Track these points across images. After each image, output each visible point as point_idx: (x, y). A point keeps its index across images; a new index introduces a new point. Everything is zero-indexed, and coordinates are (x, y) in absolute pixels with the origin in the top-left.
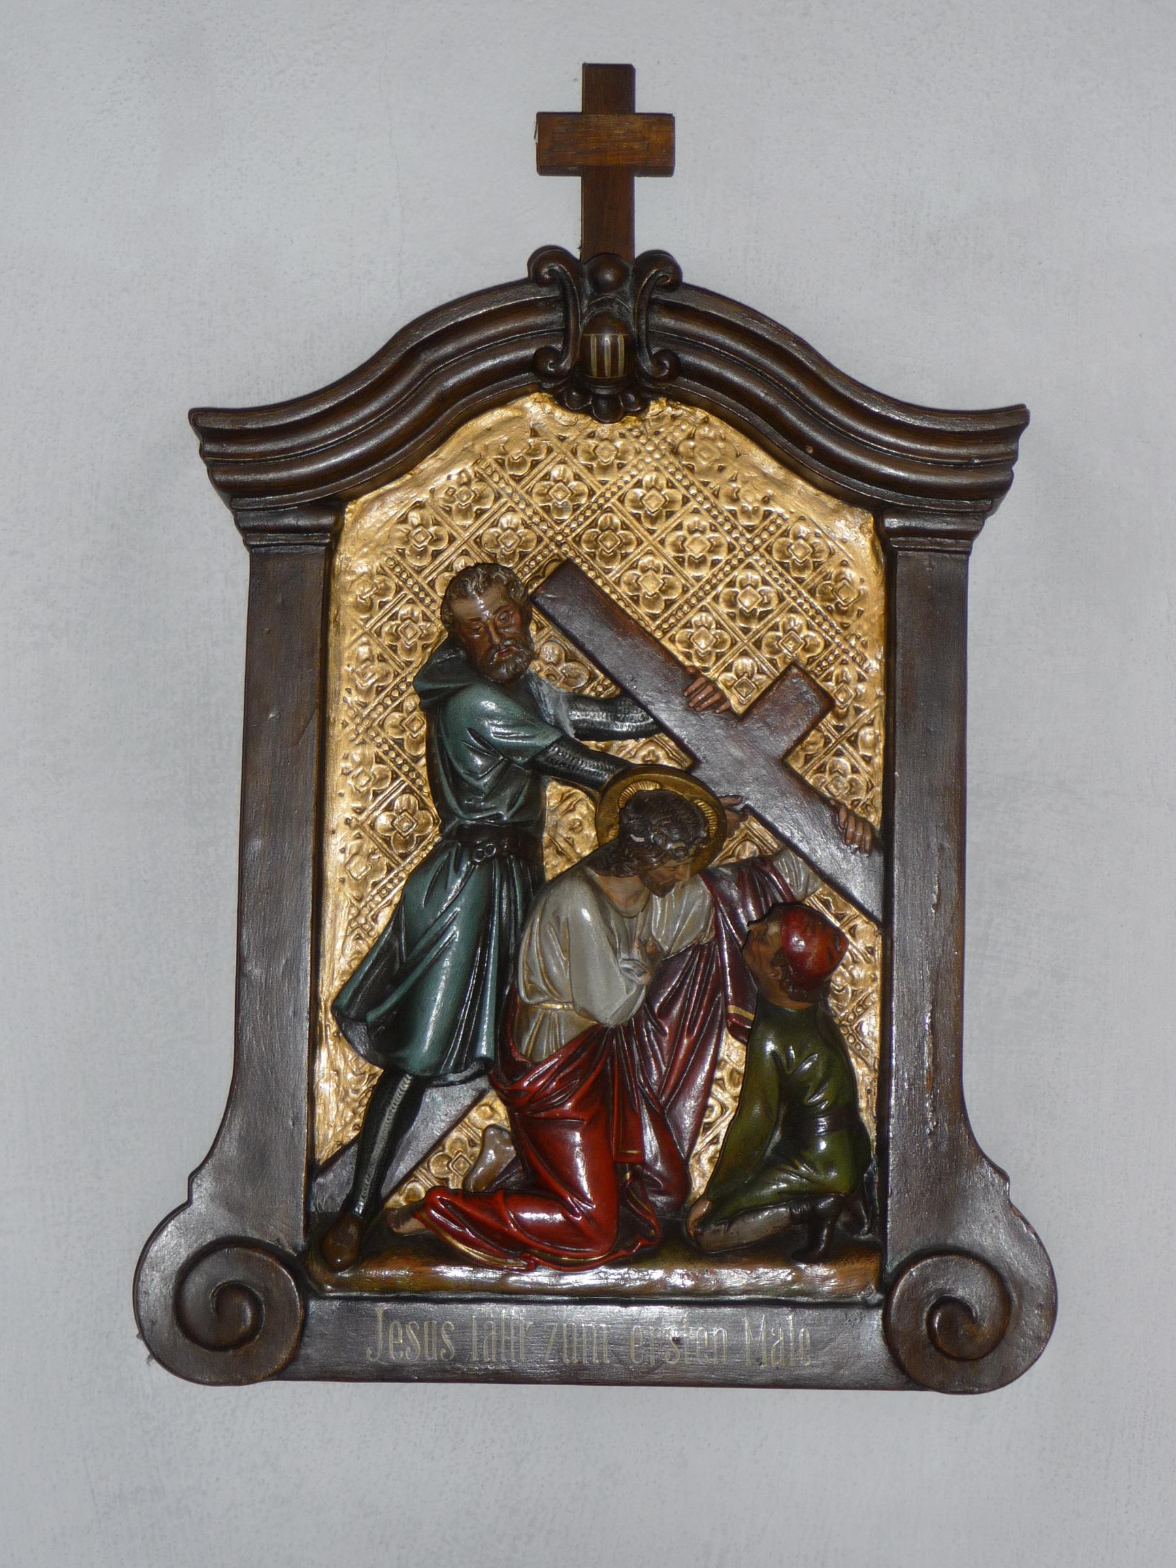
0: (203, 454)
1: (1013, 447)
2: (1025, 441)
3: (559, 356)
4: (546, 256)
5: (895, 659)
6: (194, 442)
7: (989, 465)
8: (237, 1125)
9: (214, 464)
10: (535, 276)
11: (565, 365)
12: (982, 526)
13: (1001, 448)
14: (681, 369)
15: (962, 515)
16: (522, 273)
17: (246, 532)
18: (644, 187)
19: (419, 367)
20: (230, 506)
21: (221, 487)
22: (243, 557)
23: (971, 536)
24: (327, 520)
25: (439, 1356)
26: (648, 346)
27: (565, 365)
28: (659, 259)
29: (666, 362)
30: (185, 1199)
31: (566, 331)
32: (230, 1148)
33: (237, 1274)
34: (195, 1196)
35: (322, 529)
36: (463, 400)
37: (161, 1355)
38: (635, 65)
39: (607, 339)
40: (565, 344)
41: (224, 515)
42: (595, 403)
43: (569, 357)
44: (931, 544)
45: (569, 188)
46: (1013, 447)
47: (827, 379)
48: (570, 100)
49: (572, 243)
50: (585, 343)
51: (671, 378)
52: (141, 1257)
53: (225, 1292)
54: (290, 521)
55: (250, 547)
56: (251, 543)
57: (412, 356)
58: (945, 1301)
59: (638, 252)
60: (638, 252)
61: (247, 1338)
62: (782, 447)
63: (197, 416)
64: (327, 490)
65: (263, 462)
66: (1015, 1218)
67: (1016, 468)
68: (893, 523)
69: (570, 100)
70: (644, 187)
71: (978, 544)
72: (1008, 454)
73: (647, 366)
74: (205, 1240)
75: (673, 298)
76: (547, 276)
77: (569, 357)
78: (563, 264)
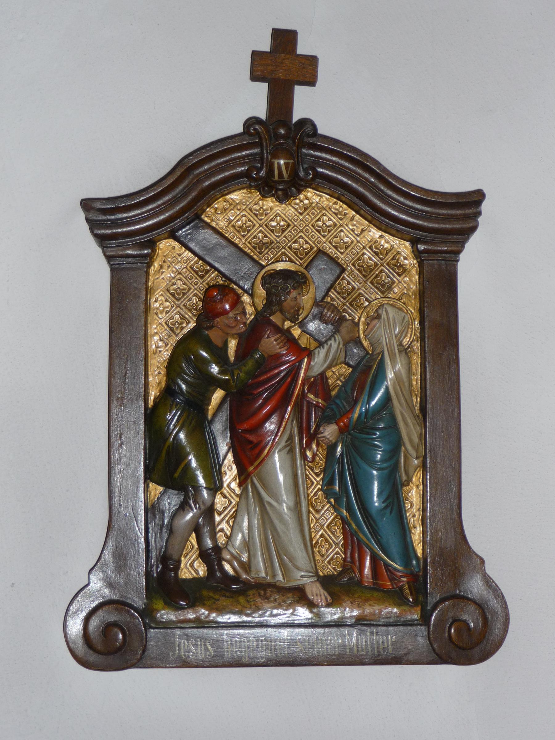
0: (87, 220)
2: (485, 206)
3: (259, 170)
4: (250, 123)
5: (423, 268)
6: (81, 216)
7: (466, 218)
8: (110, 546)
9: (93, 224)
11: (262, 173)
12: (463, 247)
14: (318, 175)
16: (240, 130)
17: (109, 258)
18: (299, 91)
21: (96, 236)
23: (458, 252)
27: (262, 173)
28: (304, 122)
29: (310, 172)
31: (262, 158)
32: (108, 556)
33: (113, 618)
34: (91, 581)
35: (146, 256)
39: (282, 162)
41: (99, 251)
42: (276, 192)
44: (440, 257)
45: (264, 87)
48: (265, 46)
49: (262, 114)
50: (272, 164)
51: (313, 179)
52: (104, 544)
54: (130, 252)
55: (111, 266)
59: (295, 119)
61: (119, 649)
62: (367, 210)
65: (384, 198)
66: (488, 581)
67: (480, 219)
68: (421, 247)
69: (265, 46)
70: (299, 91)
71: (462, 256)
73: (302, 174)
78: (260, 125)
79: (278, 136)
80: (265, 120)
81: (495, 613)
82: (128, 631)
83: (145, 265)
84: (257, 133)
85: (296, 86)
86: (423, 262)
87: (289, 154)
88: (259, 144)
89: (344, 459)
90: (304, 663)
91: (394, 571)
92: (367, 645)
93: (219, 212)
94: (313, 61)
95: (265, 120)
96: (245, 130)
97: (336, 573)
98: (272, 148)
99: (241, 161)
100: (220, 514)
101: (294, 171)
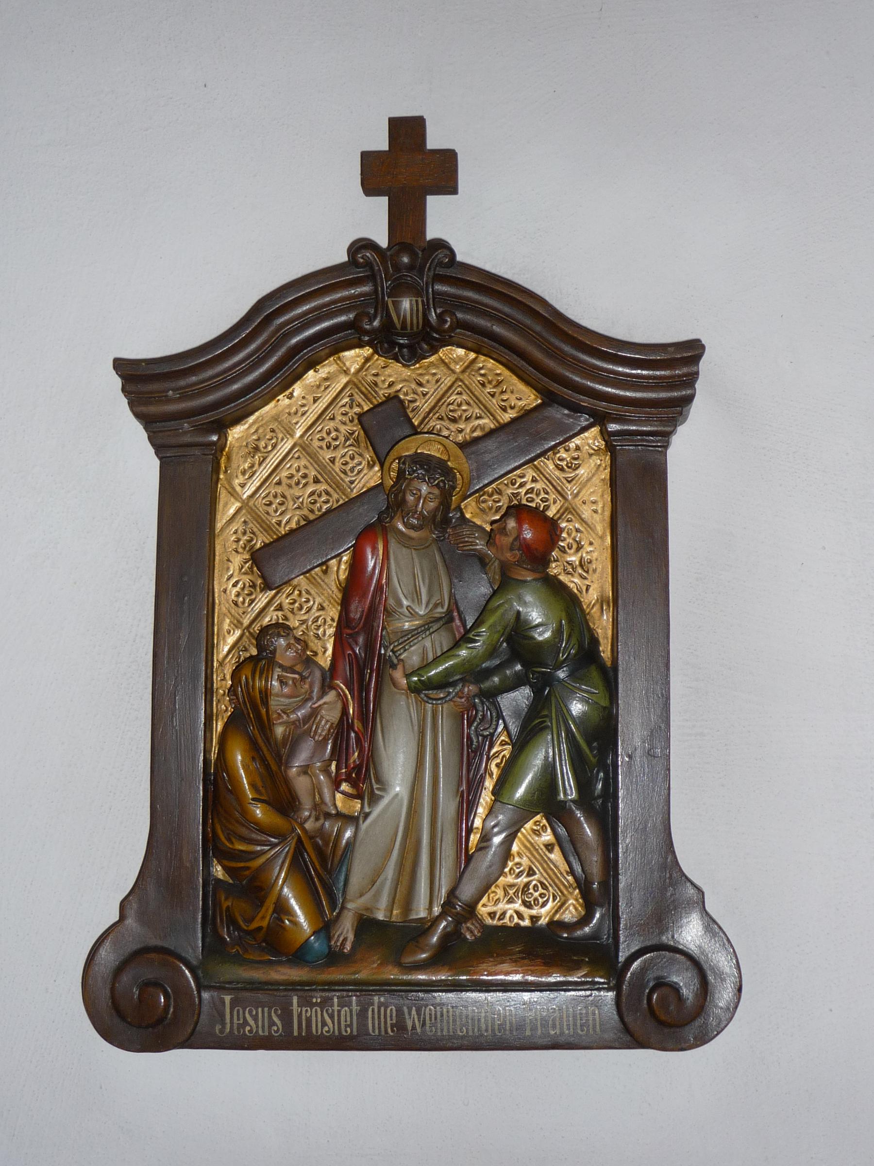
1: (694, 369)
2: (704, 365)
11: (376, 323)
13: (685, 370)
16: (343, 258)
17: (159, 448)
18: (432, 201)
19: (272, 328)
20: (146, 429)
22: (157, 462)
23: (666, 436)
25: (270, 1032)
27: (376, 323)
28: (441, 245)
33: (149, 974)
36: (243, 399)
37: (107, 1034)
43: (378, 319)
46: (694, 369)
47: (560, 325)
48: (381, 142)
51: (452, 328)
53: (147, 985)
57: (269, 319)
58: (661, 984)
63: (120, 365)
64: (212, 416)
66: (711, 925)
67: (697, 386)
68: (613, 427)
69: (381, 142)
70: (432, 201)
75: (450, 272)
76: (361, 260)
77: (378, 319)
79: (397, 267)
81: (721, 976)
84: (368, 264)
85: (428, 197)
87: (416, 291)
88: (372, 278)
89: (483, 764)
90: (360, 1047)
96: (351, 258)
97: (236, 1033)
98: (391, 284)
100: (449, 460)
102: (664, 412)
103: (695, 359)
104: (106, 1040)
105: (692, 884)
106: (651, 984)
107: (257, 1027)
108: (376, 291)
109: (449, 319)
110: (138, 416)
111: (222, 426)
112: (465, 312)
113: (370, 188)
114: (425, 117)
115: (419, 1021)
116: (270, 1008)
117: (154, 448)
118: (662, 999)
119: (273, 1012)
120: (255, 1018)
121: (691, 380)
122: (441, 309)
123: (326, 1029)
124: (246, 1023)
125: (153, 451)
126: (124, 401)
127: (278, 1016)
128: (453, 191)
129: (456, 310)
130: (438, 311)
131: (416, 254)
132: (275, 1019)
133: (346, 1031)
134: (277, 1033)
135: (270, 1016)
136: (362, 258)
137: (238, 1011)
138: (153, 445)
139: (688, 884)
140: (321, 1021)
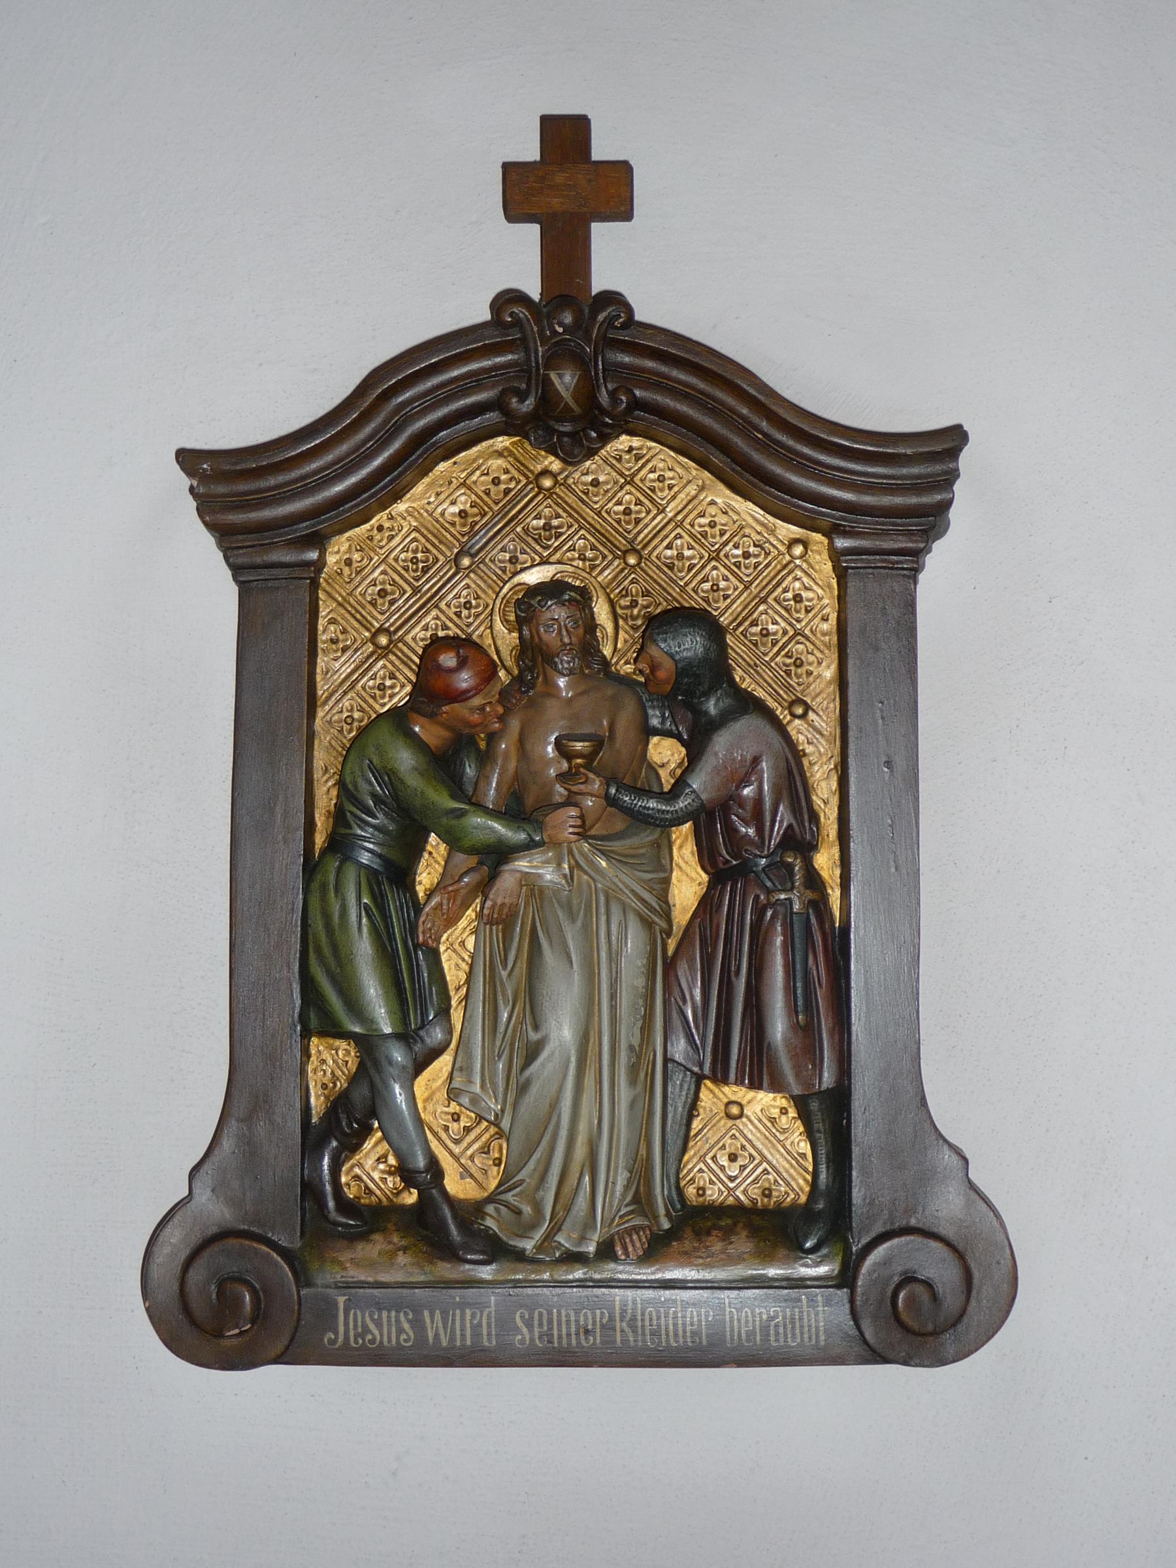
2: (965, 460)
4: (507, 299)
9: (207, 507)
10: (496, 321)
13: (938, 468)
14: (637, 404)
15: (910, 534)
16: (485, 315)
17: (237, 570)
18: (600, 231)
22: (234, 590)
23: (917, 555)
24: (314, 555)
26: (605, 382)
28: (612, 299)
30: (187, 1193)
35: (307, 564)
38: (540, 115)
40: (529, 384)
45: (533, 231)
47: (774, 408)
48: (530, 151)
56: (241, 579)
58: (909, 1279)
60: (595, 290)
63: (187, 459)
64: (304, 528)
65: (769, 446)
68: (841, 543)
69: (530, 151)
70: (600, 231)
72: (946, 473)
73: (604, 398)
74: (774, 1099)
80: (537, 300)
82: (265, 1292)
83: (308, 581)
84: (517, 323)
85: (593, 225)
86: (847, 571)
87: (580, 361)
88: (523, 343)
91: (372, 907)
92: (700, 1321)
93: (753, 874)
94: (622, 171)
95: (537, 300)
99: (475, 381)
101: (587, 391)
102: (914, 524)
103: (953, 453)
104: (177, 1356)
105: (952, 1147)
106: (896, 1279)
107: (381, 1336)
108: (528, 359)
109: (624, 398)
110: (210, 527)
111: (318, 540)
112: (646, 389)
113: (514, 211)
114: (589, 117)
115: (445, 1328)
116: (398, 1312)
117: (231, 570)
118: (910, 1299)
119: (367, 1314)
120: (379, 1325)
121: (948, 479)
122: (615, 385)
123: (403, 1336)
124: (366, 1330)
125: (229, 573)
126: (192, 504)
127: (409, 1321)
128: (627, 215)
129: (634, 387)
130: (610, 386)
131: (581, 311)
132: (406, 1326)
133: (356, 1342)
134: (371, 1344)
135: (398, 1321)
136: (511, 315)
137: (355, 1315)
138: (231, 566)
139: (946, 1147)
140: (362, 1325)
